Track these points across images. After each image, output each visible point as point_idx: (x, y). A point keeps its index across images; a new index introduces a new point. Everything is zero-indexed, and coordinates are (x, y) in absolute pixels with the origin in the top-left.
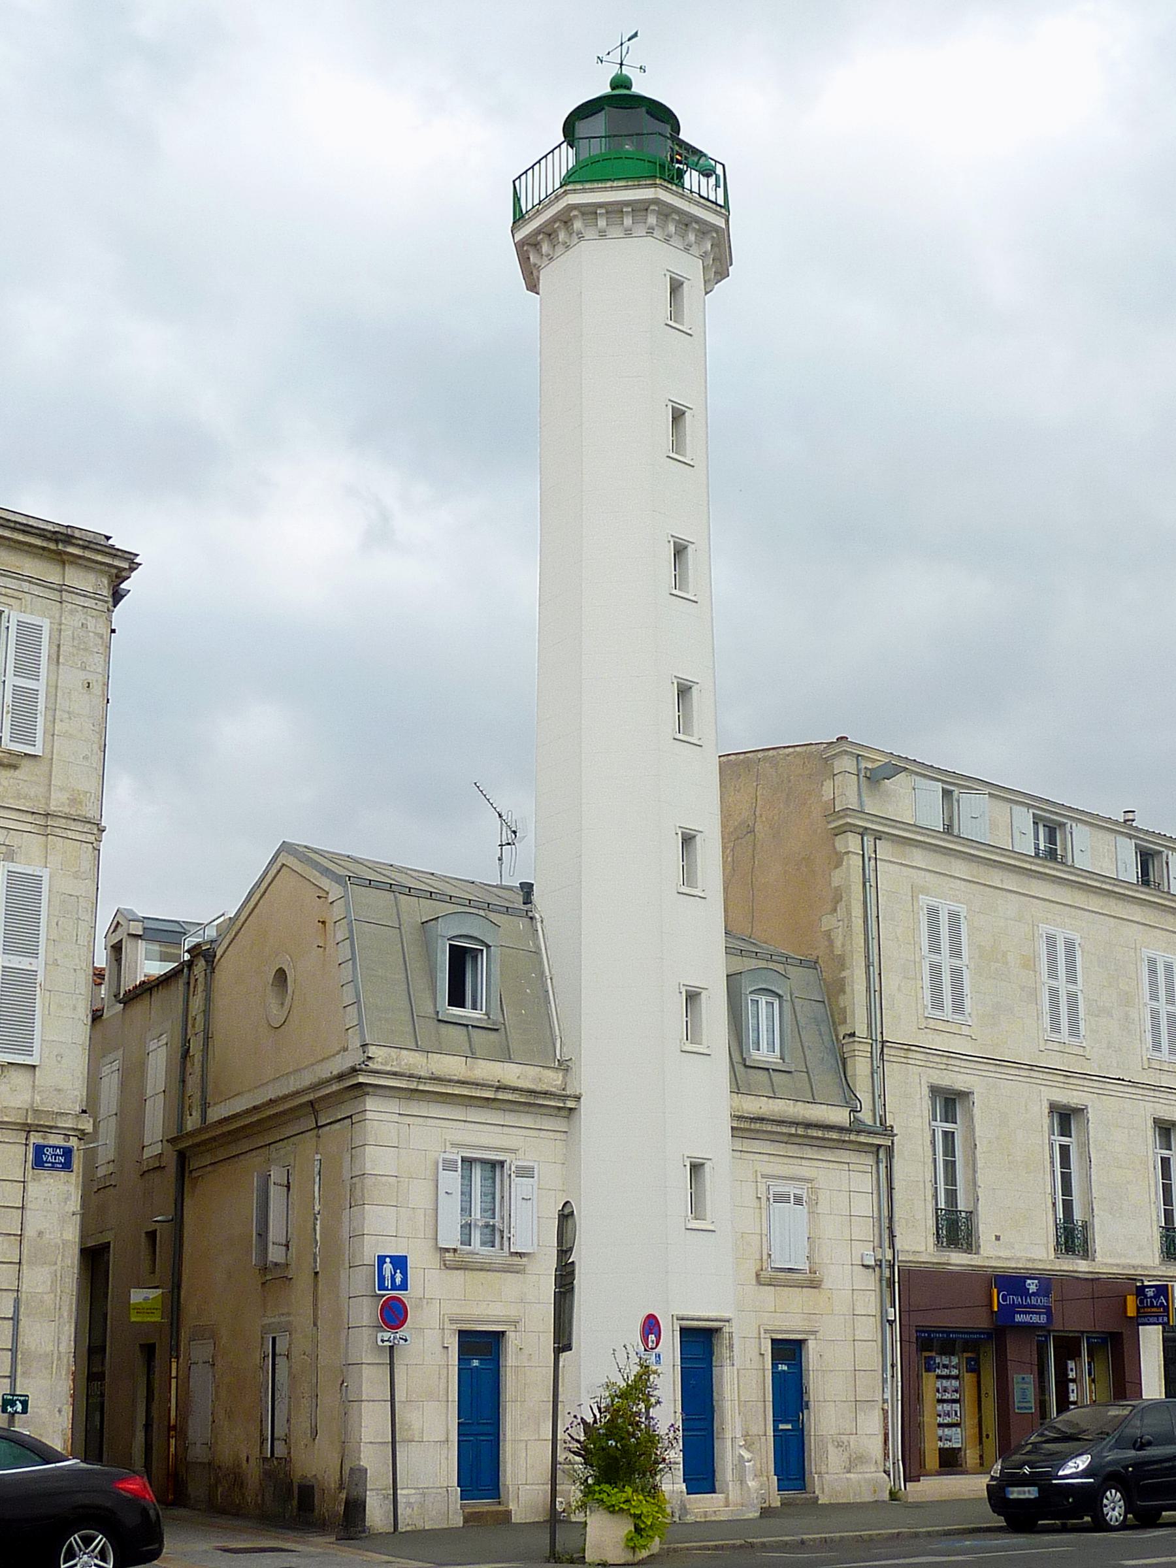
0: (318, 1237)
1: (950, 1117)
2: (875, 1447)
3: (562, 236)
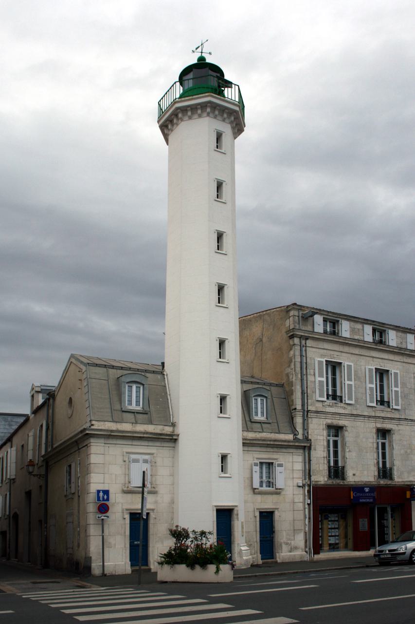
0: (79, 484)
1: (384, 437)
2: (302, 544)
3: (175, 121)
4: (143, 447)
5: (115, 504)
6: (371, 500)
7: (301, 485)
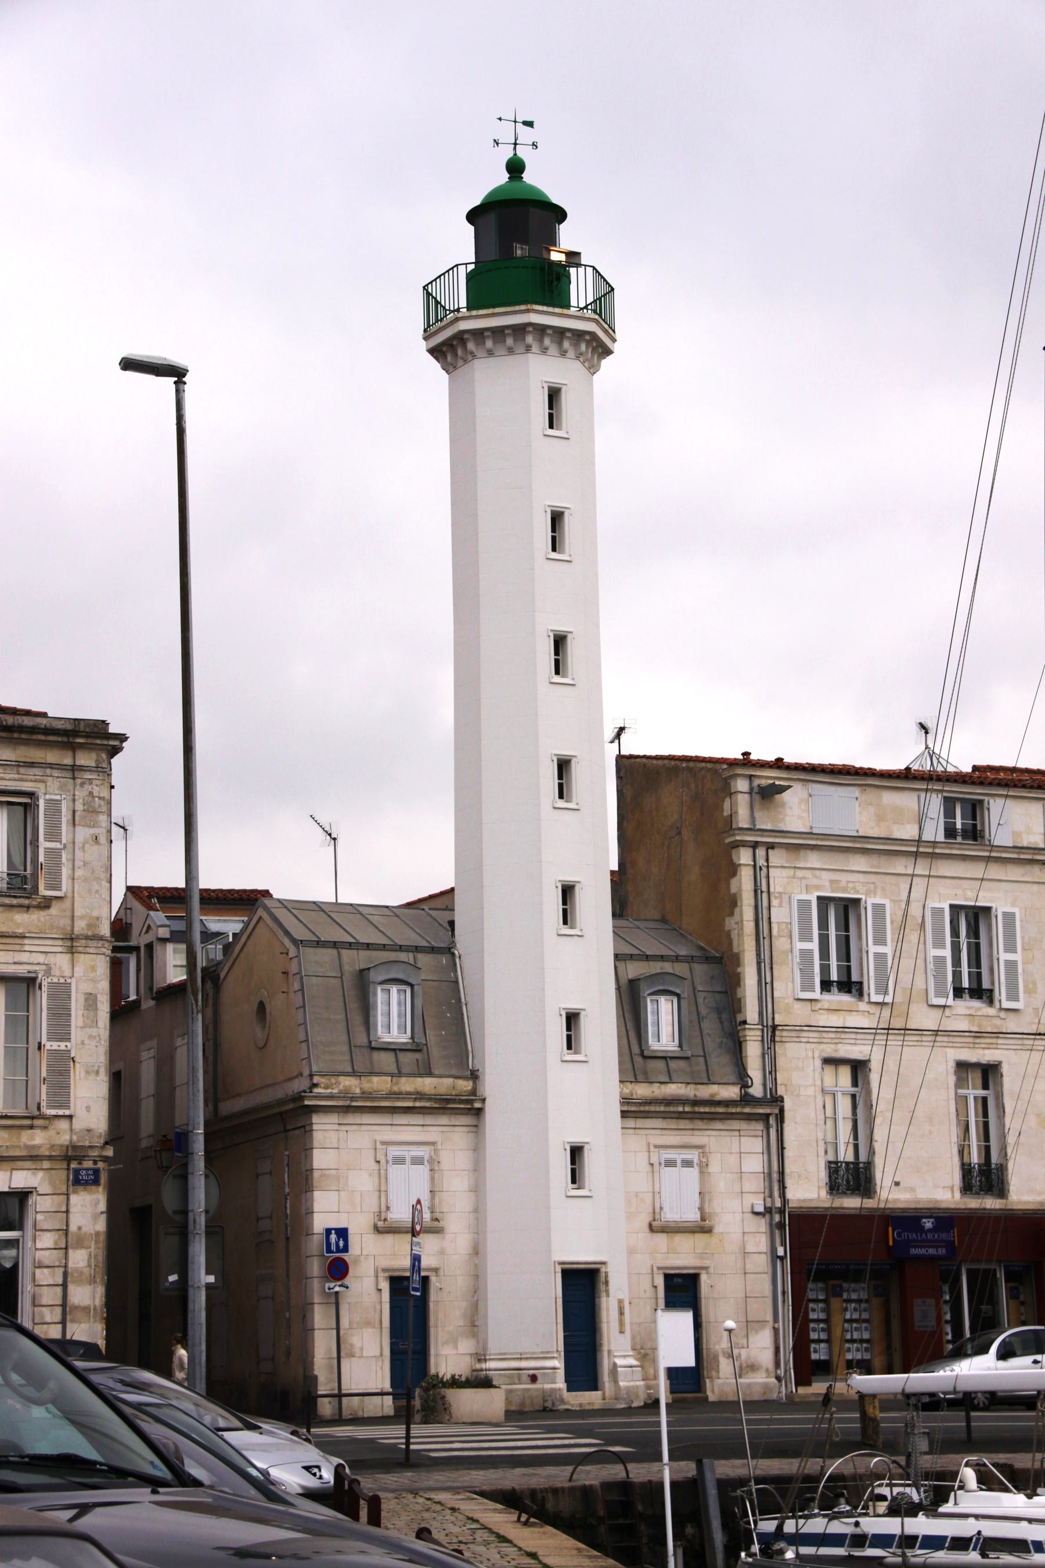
2: (766, 1358)
4: (413, 1128)
5: (362, 1258)
6: (942, 1251)
7: (761, 1209)
